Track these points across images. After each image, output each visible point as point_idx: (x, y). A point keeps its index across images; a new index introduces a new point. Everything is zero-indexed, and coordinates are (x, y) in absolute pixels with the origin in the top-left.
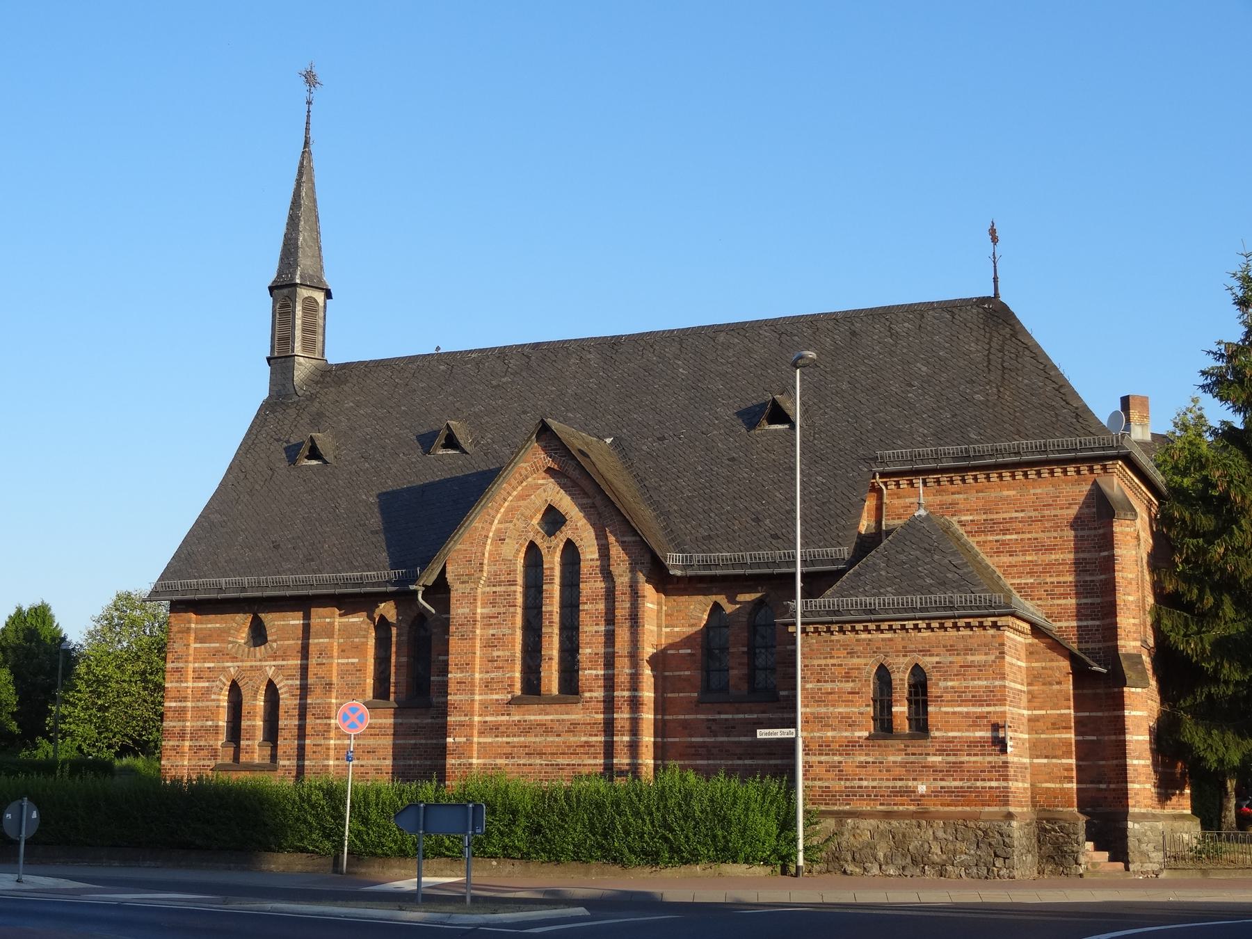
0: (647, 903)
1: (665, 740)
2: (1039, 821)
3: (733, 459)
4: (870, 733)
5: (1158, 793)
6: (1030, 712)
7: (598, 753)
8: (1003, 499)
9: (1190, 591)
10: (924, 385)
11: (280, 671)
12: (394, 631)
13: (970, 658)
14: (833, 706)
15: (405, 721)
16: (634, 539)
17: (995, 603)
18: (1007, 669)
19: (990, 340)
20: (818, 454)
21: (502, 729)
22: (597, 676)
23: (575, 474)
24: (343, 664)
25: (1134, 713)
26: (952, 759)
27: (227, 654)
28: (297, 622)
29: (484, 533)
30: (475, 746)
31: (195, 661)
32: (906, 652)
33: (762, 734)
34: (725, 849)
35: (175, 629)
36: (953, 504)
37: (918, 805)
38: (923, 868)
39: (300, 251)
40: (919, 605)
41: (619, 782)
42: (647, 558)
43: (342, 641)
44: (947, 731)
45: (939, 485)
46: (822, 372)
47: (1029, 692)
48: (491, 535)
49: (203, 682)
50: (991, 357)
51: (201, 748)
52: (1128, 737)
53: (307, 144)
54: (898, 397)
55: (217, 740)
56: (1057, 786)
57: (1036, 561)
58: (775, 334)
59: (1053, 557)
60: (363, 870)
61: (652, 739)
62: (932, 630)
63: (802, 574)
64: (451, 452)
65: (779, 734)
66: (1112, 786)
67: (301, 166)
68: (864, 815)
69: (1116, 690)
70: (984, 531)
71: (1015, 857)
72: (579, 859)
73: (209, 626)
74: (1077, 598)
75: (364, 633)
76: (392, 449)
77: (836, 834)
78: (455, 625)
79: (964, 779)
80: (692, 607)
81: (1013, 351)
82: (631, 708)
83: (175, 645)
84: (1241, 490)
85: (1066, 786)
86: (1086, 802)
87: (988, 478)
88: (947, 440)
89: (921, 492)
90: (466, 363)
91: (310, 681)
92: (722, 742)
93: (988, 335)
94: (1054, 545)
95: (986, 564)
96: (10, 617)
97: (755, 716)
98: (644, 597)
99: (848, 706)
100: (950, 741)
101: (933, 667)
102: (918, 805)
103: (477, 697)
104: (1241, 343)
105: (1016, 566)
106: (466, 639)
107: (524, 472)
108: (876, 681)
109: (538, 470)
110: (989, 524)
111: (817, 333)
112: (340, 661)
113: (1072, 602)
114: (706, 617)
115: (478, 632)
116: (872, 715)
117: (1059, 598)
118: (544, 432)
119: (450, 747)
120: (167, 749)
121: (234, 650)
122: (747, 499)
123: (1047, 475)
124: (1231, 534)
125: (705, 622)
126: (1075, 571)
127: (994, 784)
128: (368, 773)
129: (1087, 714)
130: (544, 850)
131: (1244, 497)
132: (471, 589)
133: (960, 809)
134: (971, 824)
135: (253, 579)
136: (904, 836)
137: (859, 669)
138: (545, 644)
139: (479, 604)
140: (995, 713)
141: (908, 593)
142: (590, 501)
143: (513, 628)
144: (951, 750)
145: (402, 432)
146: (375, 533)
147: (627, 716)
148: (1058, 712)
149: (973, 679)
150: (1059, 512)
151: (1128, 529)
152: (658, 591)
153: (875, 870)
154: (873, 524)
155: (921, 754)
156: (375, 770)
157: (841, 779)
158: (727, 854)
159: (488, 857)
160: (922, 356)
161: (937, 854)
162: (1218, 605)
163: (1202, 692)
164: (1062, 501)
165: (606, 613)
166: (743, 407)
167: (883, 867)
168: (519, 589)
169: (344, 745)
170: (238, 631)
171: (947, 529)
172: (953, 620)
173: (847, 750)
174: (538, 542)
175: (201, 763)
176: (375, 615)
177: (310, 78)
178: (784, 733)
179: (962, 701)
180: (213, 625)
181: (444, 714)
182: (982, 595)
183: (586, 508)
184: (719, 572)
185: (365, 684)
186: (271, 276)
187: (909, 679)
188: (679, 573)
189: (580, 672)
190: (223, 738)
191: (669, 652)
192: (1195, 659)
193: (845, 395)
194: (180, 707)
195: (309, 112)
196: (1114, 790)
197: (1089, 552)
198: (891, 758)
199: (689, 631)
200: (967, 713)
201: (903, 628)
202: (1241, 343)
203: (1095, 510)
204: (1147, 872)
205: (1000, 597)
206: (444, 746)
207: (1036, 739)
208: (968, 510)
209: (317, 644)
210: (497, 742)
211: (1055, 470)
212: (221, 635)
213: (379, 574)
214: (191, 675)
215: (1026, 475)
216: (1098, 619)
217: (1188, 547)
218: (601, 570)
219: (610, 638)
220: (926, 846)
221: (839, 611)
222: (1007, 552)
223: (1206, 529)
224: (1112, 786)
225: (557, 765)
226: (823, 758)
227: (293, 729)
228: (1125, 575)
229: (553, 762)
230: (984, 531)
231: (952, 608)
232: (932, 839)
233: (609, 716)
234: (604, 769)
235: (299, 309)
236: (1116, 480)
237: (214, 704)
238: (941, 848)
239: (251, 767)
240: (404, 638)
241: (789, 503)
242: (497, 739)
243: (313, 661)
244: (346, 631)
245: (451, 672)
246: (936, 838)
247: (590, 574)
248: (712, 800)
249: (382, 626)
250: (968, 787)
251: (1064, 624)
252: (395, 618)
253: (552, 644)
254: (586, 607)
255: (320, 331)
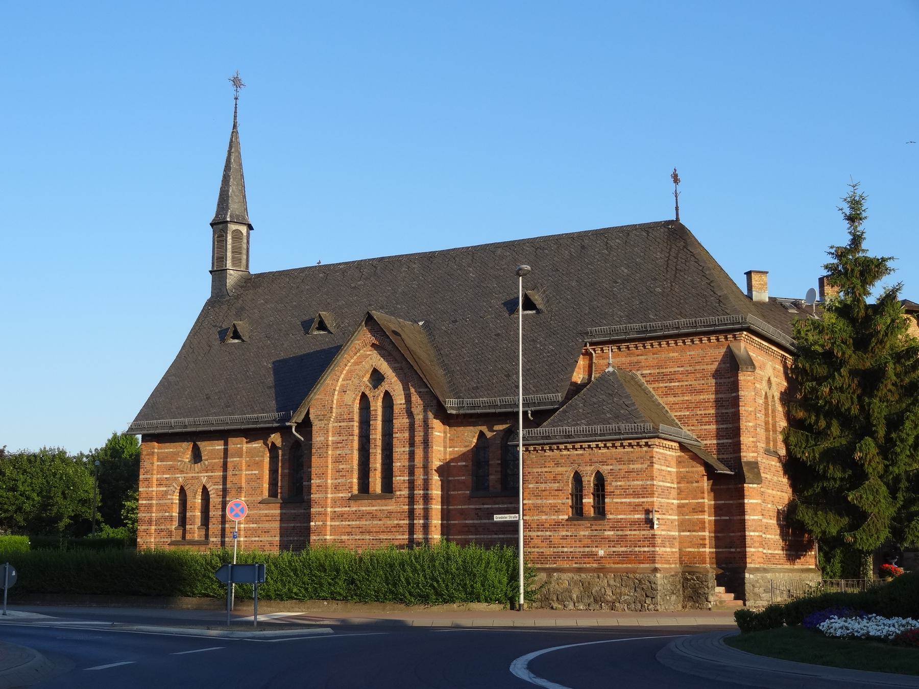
0: (398, 627)
1: (449, 522)
2: (684, 573)
3: (498, 335)
4: (569, 516)
5: (786, 555)
6: (679, 502)
7: (405, 532)
8: (670, 359)
9: (810, 417)
10: (625, 282)
11: (210, 480)
12: (280, 452)
13: (631, 466)
14: (546, 499)
15: (288, 511)
16: (426, 390)
17: (647, 429)
18: (656, 473)
19: (670, 250)
20: (552, 330)
21: (345, 516)
22: (404, 480)
23: (390, 347)
24: (249, 474)
25: (751, 501)
26: (620, 533)
27: (178, 469)
28: (220, 447)
29: (333, 388)
30: (328, 528)
31: (158, 473)
32: (591, 463)
33: (498, 518)
34: (472, 593)
35: (144, 453)
36: (638, 362)
37: (599, 563)
38: (601, 604)
39: (230, 199)
40: (599, 432)
41: (417, 549)
42: (435, 402)
43: (248, 459)
44: (617, 514)
45: (629, 350)
46: (560, 275)
47: (678, 488)
48: (337, 388)
49: (163, 487)
50: (669, 262)
51: (162, 530)
52: (747, 517)
53: (235, 126)
54: (607, 291)
55: (171, 525)
56: (696, 550)
57: (691, 400)
58: (533, 249)
59: (702, 397)
60: (245, 608)
61: (440, 522)
62: (608, 448)
63: (523, 412)
64: (322, 332)
65: (508, 517)
66: (738, 550)
67: (231, 141)
68: (565, 570)
69: (740, 486)
70: (657, 381)
71: (659, 597)
72: (378, 600)
73: (166, 450)
74: (717, 424)
75: (261, 454)
76: (286, 331)
77: (547, 583)
78: (315, 448)
79: (627, 546)
80: (466, 434)
81: (684, 257)
82: (425, 502)
83: (145, 463)
84: (842, 349)
85: (701, 550)
86: (720, 560)
87: (660, 345)
88: (635, 320)
89: (610, 356)
90: (336, 272)
91: (228, 486)
92: (485, 523)
93: (669, 247)
94: (702, 389)
95: (659, 403)
96: (109, 440)
97: (506, 506)
98: (433, 428)
99: (555, 499)
100: (619, 521)
101: (609, 473)
102: (599, 563)
103: (329, 496)
104: (848, 247)
105: (678, 404)
106: (322, 457)
107: (357, 347)
108: (574, 482)
109: (366, 345)
110: (661, 375)
111: (560, 248)
112: (247, 472)
113: (713, 427)
114: (475, 440)
115: (330, 452)
116: (570, 504)
117: (705, 425)
118: (370, 320)
119: (313, 528)
120: (141, 531)
121: (181, 466)
122: (504, 362)
123: (698, 342)
124: (834, 378)
125: (474, 444)
126: (715, 406)
127: (646, 549)
128: (265, 546)
129: (723, 502)
130: (356, 595)
131: (844, 353)
132: (325, 424)
133: (625, 566)
134: (631, 576)
135: (191, 419)
136: (589, 583)
137: (562, 474)
138: (372, 460)
139: (330, 434)
140: (647, 502)
141: (595, 423)
142: (399, 365)
143: (352, 450)
144: (619, 527)
145: (292, 319)
146: (270, 387)
147: (422, 507)
148: (697, 501)
149: (633, 480)
150: (705, 367)
151: (749, 378)
152: (444, 424)
153: (571, 606)
154: (587, 377)
155: (601, 530)
156: (269, 544)
157: (551, 547)
158: (473, 596)
159: (322, 599)
160: (625, 262)
161: (609, 595)
162: (829, 426)
163: (818, 486)
164: (707, 360)
165: (409, 439)
166: (508, 299)
167: (576, 604)
168: (356, 424)
169: (249, 527)
170: (184, 453)
171: (633, 378)
172: (620, 442)
173: (554, 528)
174: (367, 393)
175: (162, 540)
176: (268, 442)
177: (236, 82)
178: (511, 517)
179: (626, 495)
180: (169, 450)
181: (310, 507)
182: (639, 424)
183: (397, 370)
184: (479, 411)
185: (262, 487)
186: (211, 215)
187: (594, 481)
188: (454, 412)
189: (394, 479)
190: (176, 524)
191: (452, 464)
192: (809, 463)
193: (574, 290)
194: (148, 504)
195: (236, 104)
196: (739, 552)
197: (725, 393)
198: (582, 533)
199: (464, 450)
200: (630, 503)
201: (589, 447)
202: (848, 247)
203: (728, 365)
204: (759, 607)
205: (650, 426)
206: (309, 528)
207: (682, 519)
208: (647, 367)
209: (233, 461)
210: (342, 525)
211: (703, 339)
212: (173, 456)
213: (268, 416)
214: (155, 482)
215: (684, 342)
216: (731, 439)
217: (805, 388)
218: (406, 411)
219: (412, 455)
220: (603, 590)
221: (572, 435)
222: (672, 394)
223: (821, 375)
224: (738, 550)
225: (379, 539)
226: (539, 533)
227: (219, 517)
228: (747, 408)
229: (377, 538)
230: (657, 381)
231: (620, 433)
232: (605, 585)
233: (412, 507)
234: (409, 542)
235: (229, 237)
236: (743, 345)
237: (170, 501)
238: (612, 591)
239: (193, 543)
240: (286, 457)
241: (529, 364)
242: (342, 523)
243: (230, 473)
244: (250, 453)
245: (313, 479)
246: (609, 585)
247: (400, 413)
248: (464, 562)
249: (273, 449)
250: (630, 552)
251: (708, 442)
252: (281, 444)
253: (376, 460)
254: (397, 435)
255: (244, 252)
